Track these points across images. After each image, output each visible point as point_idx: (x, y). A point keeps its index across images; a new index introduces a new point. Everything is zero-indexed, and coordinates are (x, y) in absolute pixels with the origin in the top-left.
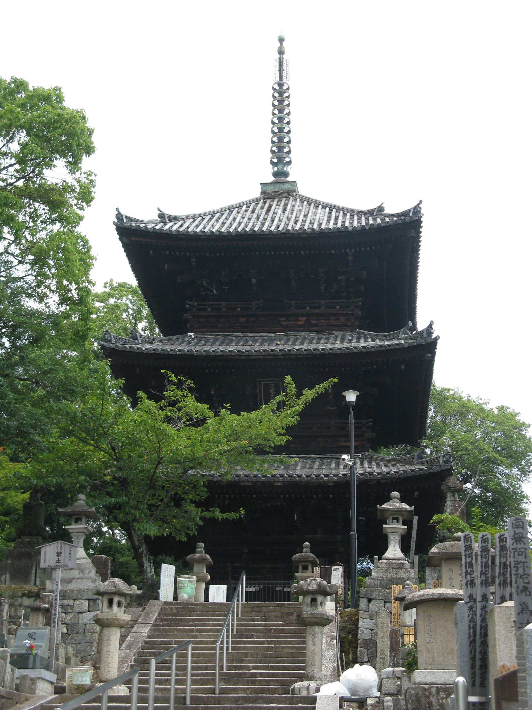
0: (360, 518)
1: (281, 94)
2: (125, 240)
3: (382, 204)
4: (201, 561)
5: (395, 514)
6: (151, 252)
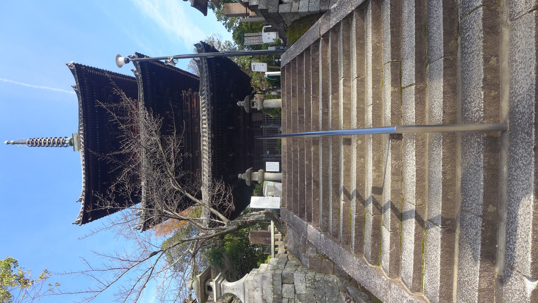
1: (34, 143)
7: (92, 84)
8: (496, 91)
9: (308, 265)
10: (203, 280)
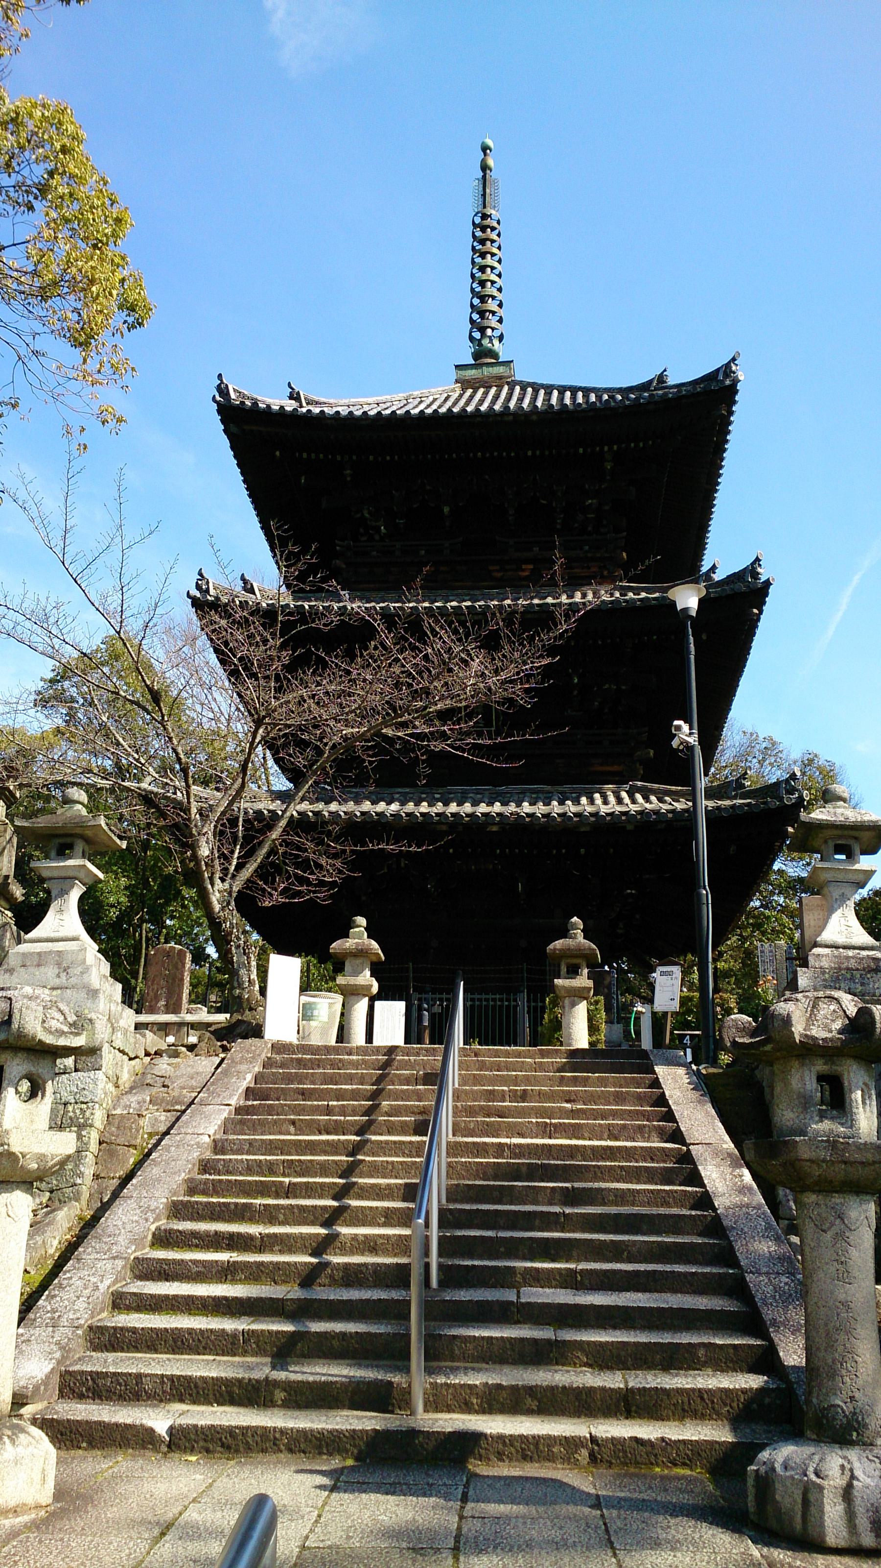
0: (629, 891)
1: (483, 229)
2: (233, 428)
3: (665, 370)
4: (360, 953)
5: (840, 837)
6: (278, 453)
7: (671, 440)
8: (480, 1406)
9: (118, 1111)
10: (88, 833)
